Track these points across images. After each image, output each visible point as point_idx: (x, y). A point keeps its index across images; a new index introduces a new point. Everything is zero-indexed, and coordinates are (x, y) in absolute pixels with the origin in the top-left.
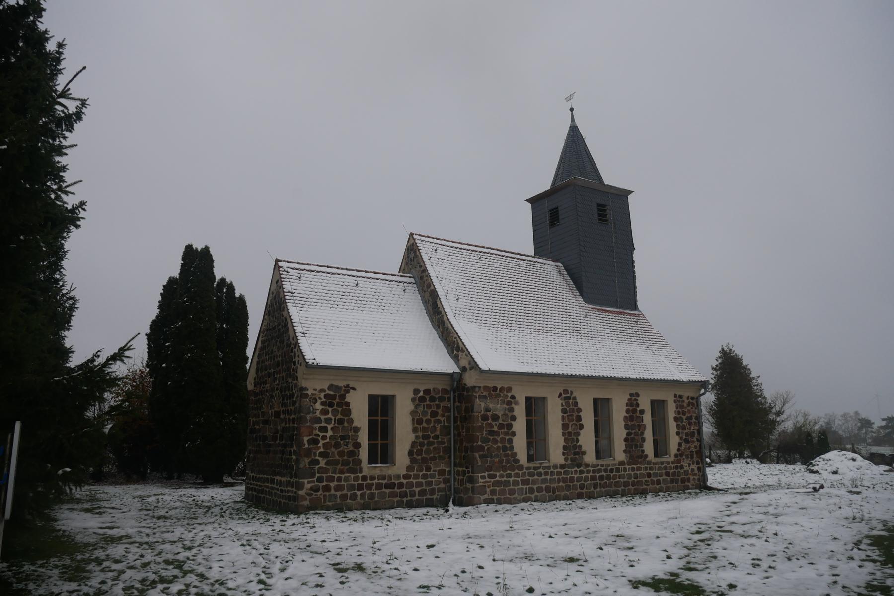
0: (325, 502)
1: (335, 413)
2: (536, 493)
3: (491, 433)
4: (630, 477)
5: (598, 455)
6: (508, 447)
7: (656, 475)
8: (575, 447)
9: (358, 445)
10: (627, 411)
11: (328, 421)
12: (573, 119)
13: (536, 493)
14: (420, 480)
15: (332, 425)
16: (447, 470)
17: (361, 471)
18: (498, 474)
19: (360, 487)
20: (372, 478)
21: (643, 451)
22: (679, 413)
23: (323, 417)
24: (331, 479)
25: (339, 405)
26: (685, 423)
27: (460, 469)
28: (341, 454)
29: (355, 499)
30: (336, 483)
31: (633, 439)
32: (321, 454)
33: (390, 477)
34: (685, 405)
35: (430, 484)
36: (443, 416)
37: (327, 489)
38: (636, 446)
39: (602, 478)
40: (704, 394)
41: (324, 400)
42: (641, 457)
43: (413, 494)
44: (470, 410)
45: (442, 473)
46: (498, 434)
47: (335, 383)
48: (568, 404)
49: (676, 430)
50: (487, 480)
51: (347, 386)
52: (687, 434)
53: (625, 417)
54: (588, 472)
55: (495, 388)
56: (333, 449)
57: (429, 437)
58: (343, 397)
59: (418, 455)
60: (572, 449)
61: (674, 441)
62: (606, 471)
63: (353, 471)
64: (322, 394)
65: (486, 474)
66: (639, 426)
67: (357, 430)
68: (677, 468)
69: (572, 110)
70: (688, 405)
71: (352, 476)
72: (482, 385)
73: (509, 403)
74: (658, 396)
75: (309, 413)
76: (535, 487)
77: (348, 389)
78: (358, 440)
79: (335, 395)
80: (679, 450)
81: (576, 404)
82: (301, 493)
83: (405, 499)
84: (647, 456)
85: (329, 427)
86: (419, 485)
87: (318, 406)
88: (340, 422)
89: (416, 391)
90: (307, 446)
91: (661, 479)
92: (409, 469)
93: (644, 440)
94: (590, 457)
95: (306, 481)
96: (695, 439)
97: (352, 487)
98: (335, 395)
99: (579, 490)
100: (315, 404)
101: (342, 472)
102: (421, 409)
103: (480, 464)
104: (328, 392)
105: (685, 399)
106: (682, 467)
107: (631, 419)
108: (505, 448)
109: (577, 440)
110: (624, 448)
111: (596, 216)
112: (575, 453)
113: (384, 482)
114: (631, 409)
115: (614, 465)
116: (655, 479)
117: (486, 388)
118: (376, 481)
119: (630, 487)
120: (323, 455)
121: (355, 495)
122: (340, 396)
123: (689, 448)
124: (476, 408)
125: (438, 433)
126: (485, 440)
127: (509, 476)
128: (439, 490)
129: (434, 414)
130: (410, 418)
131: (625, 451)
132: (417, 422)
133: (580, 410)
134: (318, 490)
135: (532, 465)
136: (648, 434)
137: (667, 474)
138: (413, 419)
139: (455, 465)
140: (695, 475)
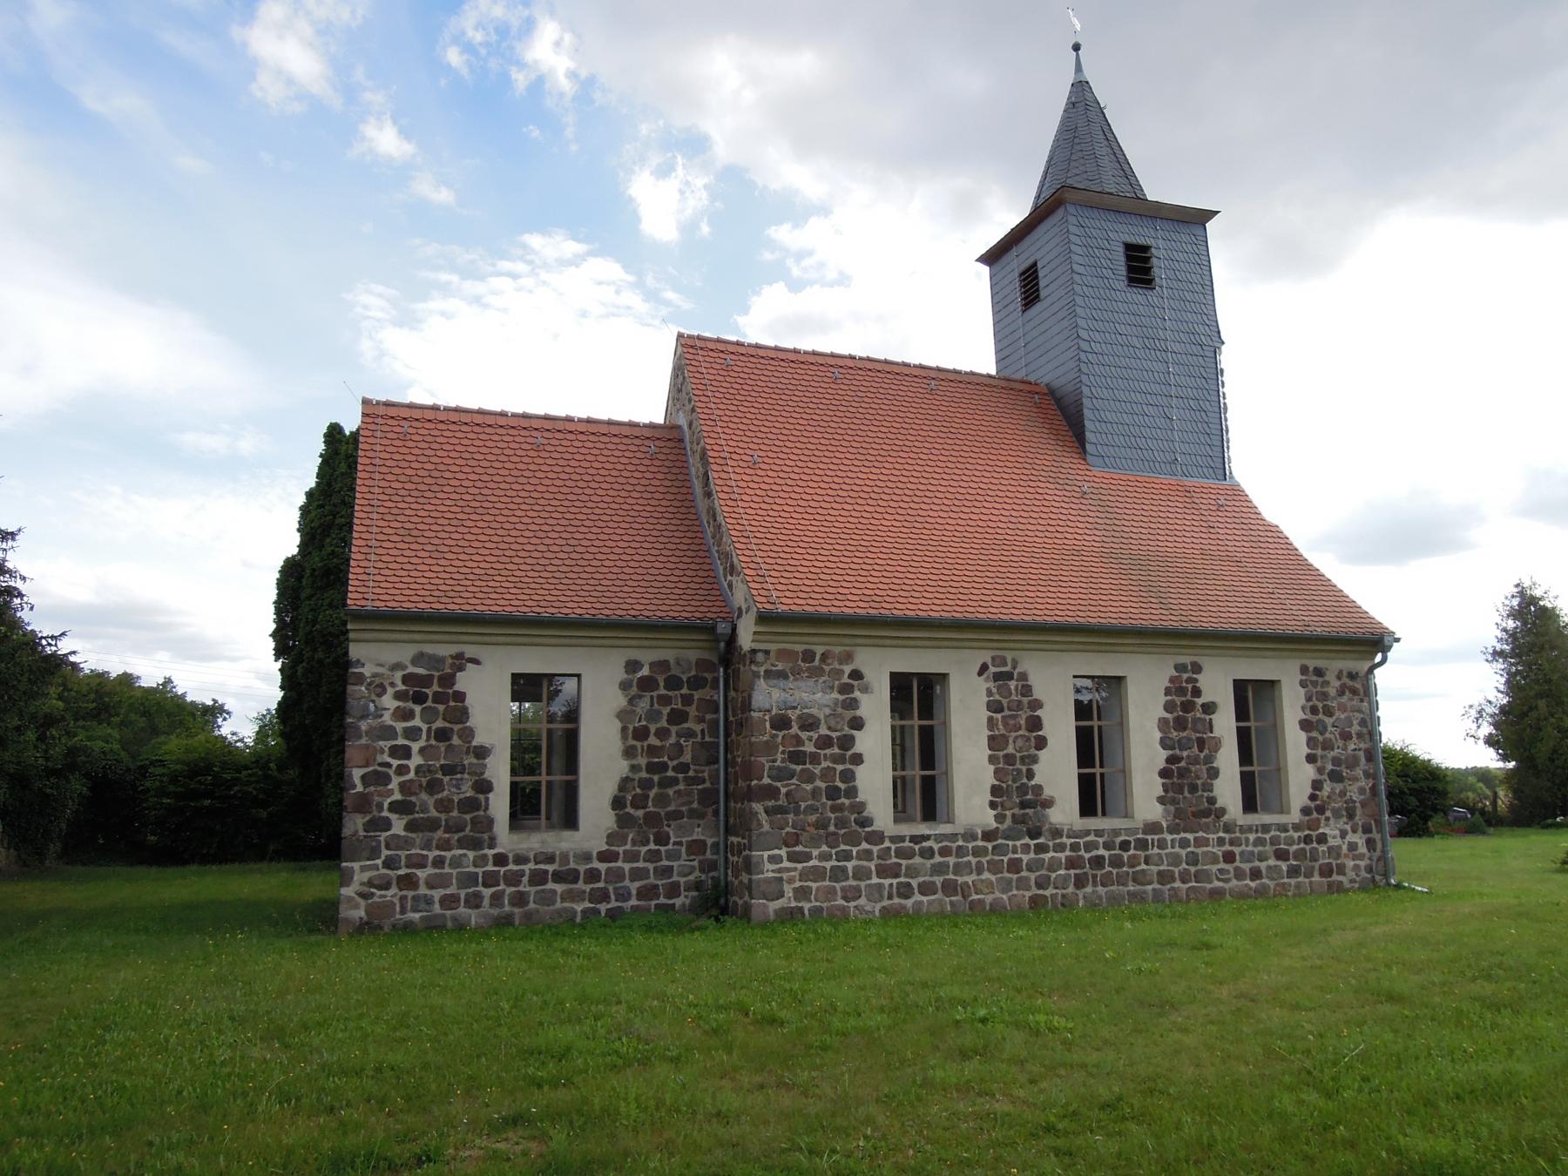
0: (403, 911)
1: (429, 715)
5: (1088, 805)
6: (842, 791)
7: (1247, 857)
8: (1023, 790)
9: (484, 787)
10: (1168, 707)
11: (413, 734)
12: (1079, 68)
13: (918, 897)
14: (641, 864)
15: (422, 743)
16: (710, 841)
18: (815, 853)
19: (490, 880)
20: (521, 859)
21: (1212, 801)
22: (1314, 710)
25: (438, 698)
28: (444, 806)
29: (478, 906)
30: (430, 871)
31: (1183, 773)
32: (396, 807)
33: (565, 857)
34: (1332, 692)
35: (667, 871)
36: (701, 720)
37: (408, 882)
38: (1193, 788)
39: (1098, 862)
41: (401, 687)
43: (624, 896)
44: (747, 706)
45: (696, 847)
46: (815, 759)
47: (429, 649)
50: (786, 864)
51: (460, 656)
52: (1336, 761)
53: (1163, 723)
54: (1060, 848)
56: (424, 796)
57: (664, 767)
58: (448, 680)
59: (635, 806)
60: (1018, 797)
61: (1299, 778)
62: (1107, 846)
63: (475, 845)
64: (399, 675)
65: (783, 852)
67: (482, 752)
68: (1307, 840)
69: (1076, 48)
70: (1341, 693)
71: (471, 854)
73: (846, 689)
74: (1255, 669)
75: (364, 717)
77: (460, 662)
80: (1313, 797)
81: (1027, 690)
82: (345, 891)
83: (603, 907)
84: (1223, 811)
85: (415, 747)
87: (389, 702)
88: (442, 735)
89: (632, 666)
90: (360, 788)
91: (1263, 865)
92: (612, 838)
93: (1214, 773)
94: (1065, 810)
95: (356, 866)
96: (1359, 772)
97: (471, 879)
100: (380, 695)
101: (445, 845)
102: (643, 705)
103: (766, 827)
104: (411, 669)
105: (1330, 677)
106: (1322, 839)
107: (1180, 724)
108: (833, 793)
110: (1160, 791)
111: (1123, 271)
112: (1023, 805)
113: (550, 868)
114: (1178, 700)
115: (1129, 831)
116: (1246, 867)
118: (531, 866)
121: (478, 896)
123: (1343, 793)
125: (687, 757)
126: (781, 775)
127: (847, 856)
129: (677, 717)
131: (1161, 800)
132: (635, 735)
133: (1037, 705)
134: (386, 887)
135: (906, 830)
137: (1281, 855)
138: (624, 729)
139: (728, 831)
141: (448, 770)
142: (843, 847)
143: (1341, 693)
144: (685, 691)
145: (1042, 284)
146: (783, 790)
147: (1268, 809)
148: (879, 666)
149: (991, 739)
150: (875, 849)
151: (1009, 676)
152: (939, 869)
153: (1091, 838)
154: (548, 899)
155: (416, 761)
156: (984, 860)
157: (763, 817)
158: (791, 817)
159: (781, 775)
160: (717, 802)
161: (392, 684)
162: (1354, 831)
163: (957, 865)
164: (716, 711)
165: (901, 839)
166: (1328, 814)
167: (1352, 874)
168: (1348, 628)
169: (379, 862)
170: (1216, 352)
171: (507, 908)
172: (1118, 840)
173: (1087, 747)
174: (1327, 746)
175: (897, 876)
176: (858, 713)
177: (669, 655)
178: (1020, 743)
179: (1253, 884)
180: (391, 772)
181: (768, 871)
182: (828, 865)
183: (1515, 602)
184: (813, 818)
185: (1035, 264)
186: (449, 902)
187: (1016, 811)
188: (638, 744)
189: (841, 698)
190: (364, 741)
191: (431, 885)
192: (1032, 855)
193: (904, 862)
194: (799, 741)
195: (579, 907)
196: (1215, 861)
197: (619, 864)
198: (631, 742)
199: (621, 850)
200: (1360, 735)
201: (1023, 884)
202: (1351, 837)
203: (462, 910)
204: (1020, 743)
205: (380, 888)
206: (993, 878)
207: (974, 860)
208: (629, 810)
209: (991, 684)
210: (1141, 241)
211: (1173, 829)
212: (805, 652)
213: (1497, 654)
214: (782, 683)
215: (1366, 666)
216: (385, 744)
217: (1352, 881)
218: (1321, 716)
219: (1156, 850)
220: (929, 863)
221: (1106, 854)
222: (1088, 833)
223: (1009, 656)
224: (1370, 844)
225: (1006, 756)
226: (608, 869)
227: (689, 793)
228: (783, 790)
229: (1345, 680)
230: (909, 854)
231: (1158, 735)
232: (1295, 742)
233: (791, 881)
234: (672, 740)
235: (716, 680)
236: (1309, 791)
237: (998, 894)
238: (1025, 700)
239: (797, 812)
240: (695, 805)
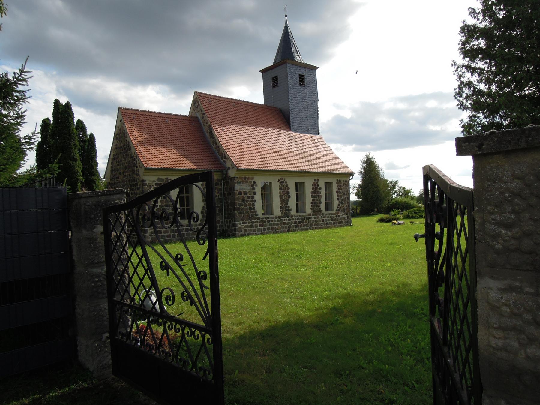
6: (252, 208)
7: (326, 220)
8: (286, 207)
10: (313, 189)
21: (320, 209)
22: (339, 189)
31: (315, 203)
36: (218, 193)
46: (247, 201)
47: (161, 177)
52: (342, 200)
54: (293, 219)
60: (285, 208)
61: (336, 203)
62: (301, 219)
64: (154, 183)
68: (337, 217)
69: (286, 16)
73: (252, 186)
74: (329, 180)
80: (338, 208)
81: (287, 185)
93: (321, 203)
96: (346, 202)
104: (157, 182)
105: (342, 182)
106: (339, 216)
107: (315, 192)
108: (251, 209)
112: (286, 211)
115: (306, 216)
126: (241, 205)
127: (253, 222)
133: (289, 188)
135: (265, 217)
137: (332, 220)
139: (225, 218)
147: (330, 211)
148: (260, 182)
164: (221, 191)
168: (346, 172)
170: (317, 103)
174: (341, 197)
181: (239, 226)
183: (365, 159)
184: (247, 214)
186: (169, 236)
191: (164, 233)
202: (344, 216)
210: (302, 74)
213: (361, 172)
223: (283, 178)
224: (348, 217)
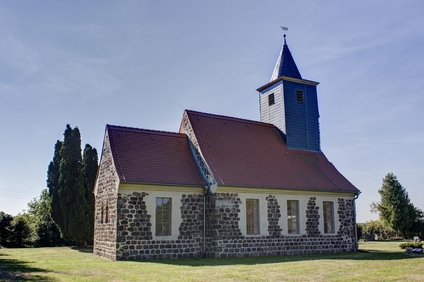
0: (131, 254)
1: (137, 207)
2: (252, 252)
3: (225, 218)
4: (309, 244)
6: (235, 226)
7: (325, 243)
8: (275, 227)
9: (149, 225)
11: (133, 212)
13: (252, 252)
14: (186, 244)
15: (135, 214)
16: (201, 238)
17: (151, 239)
18: (229, 241)
19: (151, 247)
20: (158, 242)
21: (318, 230)
22: (341, 209)
23: (130, 210)
24: (134, 243)
25: (139, 203)
26: (345, 214)
27: (209, 238)
28: (140, 229)
30: (137, 245)
31: (311, 223)
32: (129, 229)
33: (168, 242)
34: (345, 205)
35: (191, 246)
36: (199, 209)
37: (132, 247)
38: (313, 227)
39: (292, 244)
40: (357, 198)
42: (316, 233)
43: (181, 251)
44: (214, 206)
45: (198, 240)
46: (229, 219)
47: (136, 191)
48: (271, 203)
49: (339, 218)
50: (223, 244)
51: (144, 193)
52: (346, 221)
53: (307, 211)
54: (284, 240)
55: (228, 194)
56: (136, 227)
57: (191, 220)
58: (141, 199)
60: (274, 229)
61: (337, 224)
62: (294, 240)
63: (147, 238)
64: (129, 197)
65: (222, 241)
66: (315, 216)
67: (149, 216)
68: (339, 239)
69: (285, 36)
70: (347, 205)
71: (147, 241)
72: (220, 192)
73: (236, 202)
76: (251, 248)
77: (144, 194)
78: (150, 222)
79: (137, 198)
80: (340, 229)
81: (276, 203)
83: (177, 254)
84: (320, 232)
85: (134, 215)
86: (185, 246)
87: (127, 204)
88: (140, 212)
89: (184, 196)
91: (329, 245)
92: (179, 237)
93: (318, 223)
96: (351, 224)
97: (146, 247)
98: (137, 198)
99: (278, 250)
101: (141, 239)
102: (186, 205)
103: (218, 235)
104: (132, 196)
105: (345, 201)
106: (342, 239)
108: (233, 227)
109: (277, 223)
112: (276, 230)
113: (165, 244)
114: (310, 206)
115: (299, 237)
116: (325, 245)
117: (222, 194)
118: (160, 244)
119: (309, 249)
120: (129, 229)
122: (139, 198)
123: (347, 228)
124: (217, 205)
125: (196, 218)
126: (222, 222)
127: (236, 242)
128: (197, 249)
129: (194, 208)
130: (180, 210)
131: (306, 230)
132: (184, 213)
133: (279, 207)
134: (127, 248)
135: (250, 236)
136: (321, 220)
137: (333, 243)
138: (182, 211)
140: (351, 243)
141: (141, 220)
142: (235, 240)
143: (347, 205)
144: (196, 202)
145: (275, 99)
146: (222, 226)
149: (268, 215)
150: (243, 240)
151: (273, 200)
152: (257, 245)
153: (290, 238)
154: (164, 251)
155: (134, 218)
156: (267, 243)
157: (218, 232)
158: (224, 232)
159: (222, 222)
160: (203, 229)
161: (128, 200)
162: (349, 237)
163: (260, 244)
164: (203, 207)
165: (248, 238)
166: (343, 233)
167: (348, 247)
169: (125, 243)
171: (155, 254)
172: (296, 239)
173: (249, 217)
175: (247, 246)
176: (239, 208)
177: (192, 193)
178: (275, 216)
179: (326, 250)
180: (128, 221)
182: (232, 244)
185: (273, 94)
187: (274, 232)
188: (185, 215)
189: (235, 205)
190: (121, 213)
192: (277, 242)
193: (249, 243)
194: (226, 215)
195: (172, 254)
196: (318, 244)
197: (181, 244)
198: (183, 214)
199: (181, 240)
200: (351, 215)
201: (275, 249)
202: (349, 239)
203: (144, 254)
204: (275, 216)
205: (125, 249)
206: (269, 247)
207: (264, 243)
208: (183, 231)
209: (269, 202)
211: (309, 236)
212: (227, 194)
214: (222, 201)
215: (353, 198)
216: (126, 214)
217: (349, 249)
218: (342, 210)
219: (305, 241)
220: (254, 244)
221: (294, 242)
222: (290, 237)
224: (353, 240)
225: (272, 219)
226: (178, 245)
227: (196, 227)
228: (222, 226)
229: (348, 202)
230: (250, 242)
231: (306, 214)
232: (337, 216)
233: (224, 247)
234: (193, 214)
235: (203, 200)
236: (339, 228)
237: (270, 251)
238: (276, 206)
239: (225, 231)
240: (198, 230)
